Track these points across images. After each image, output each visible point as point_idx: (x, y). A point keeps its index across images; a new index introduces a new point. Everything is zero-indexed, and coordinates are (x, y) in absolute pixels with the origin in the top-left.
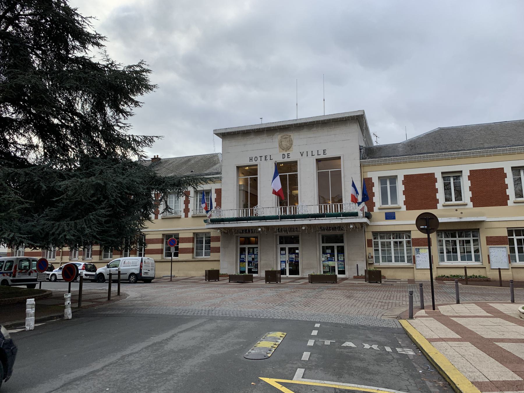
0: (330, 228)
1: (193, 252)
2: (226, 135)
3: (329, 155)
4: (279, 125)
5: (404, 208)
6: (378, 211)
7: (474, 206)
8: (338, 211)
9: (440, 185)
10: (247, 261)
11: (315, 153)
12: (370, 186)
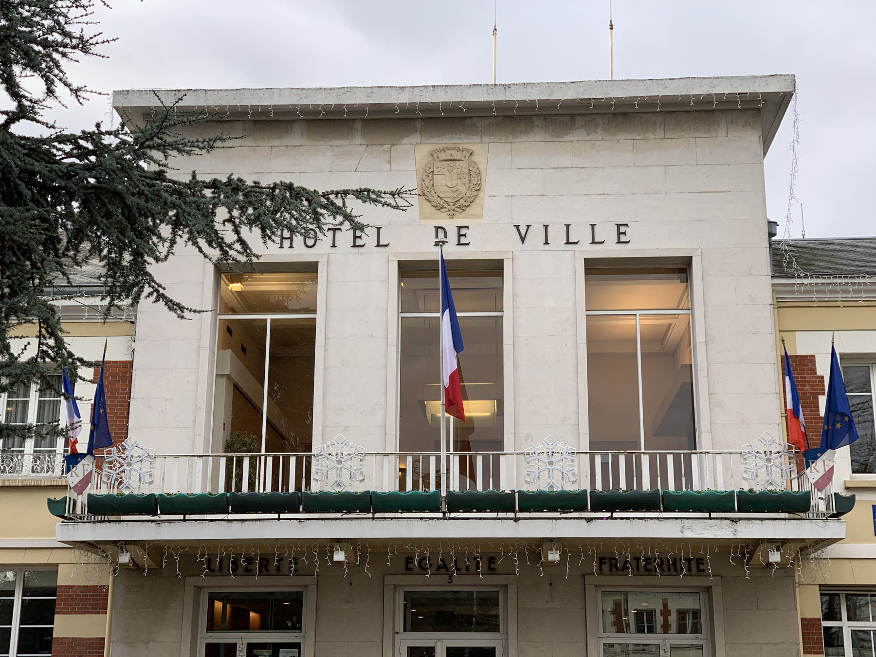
0: (249, 560)
3: (643, 244)
8: (239, 487)
11: (581, 234)
12: (808, 388)
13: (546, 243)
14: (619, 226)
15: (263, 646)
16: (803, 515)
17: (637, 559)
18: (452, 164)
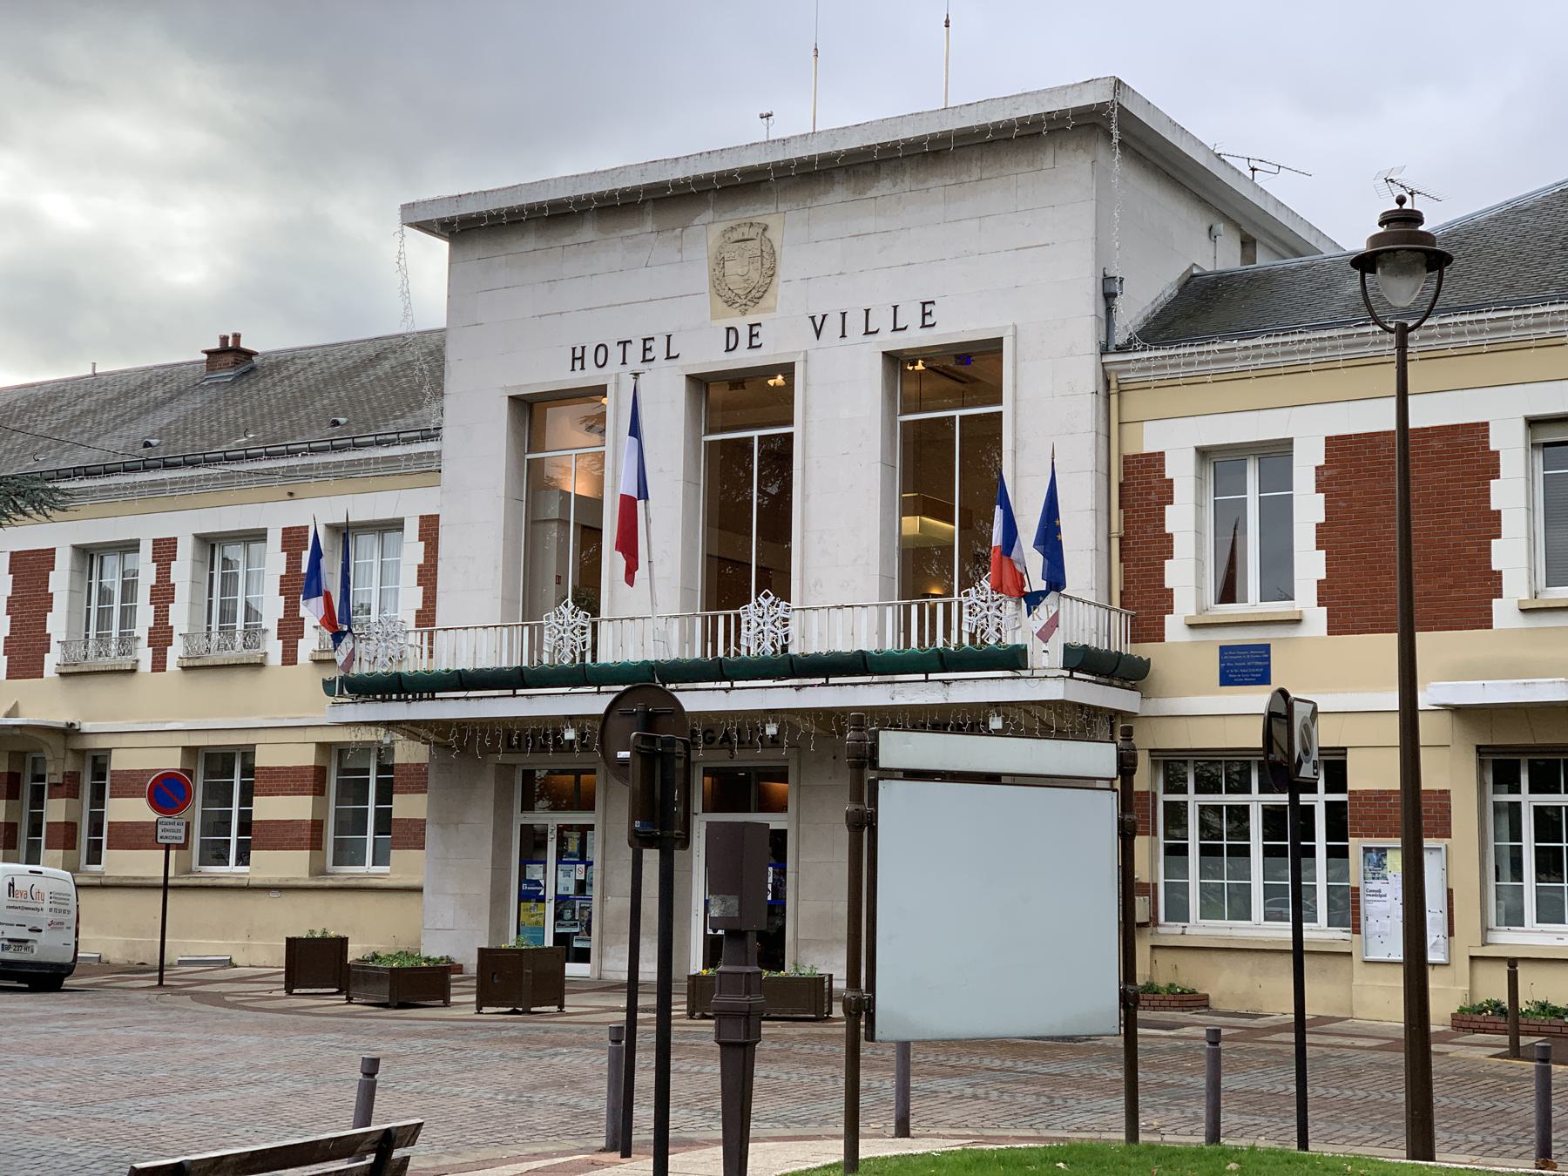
1: (316, 844)
2: (467, 229)
4: (582, 191)
5: (1317, 618)
6: (1521, 622)
7: (1332, 630)
9: (1513, 493)
10: (550, 894)
11: (881, 320)
12: (1153, 497)
13: (843, 336)
14: (924, 304)
15: (570, 827)
18: (742, 244)
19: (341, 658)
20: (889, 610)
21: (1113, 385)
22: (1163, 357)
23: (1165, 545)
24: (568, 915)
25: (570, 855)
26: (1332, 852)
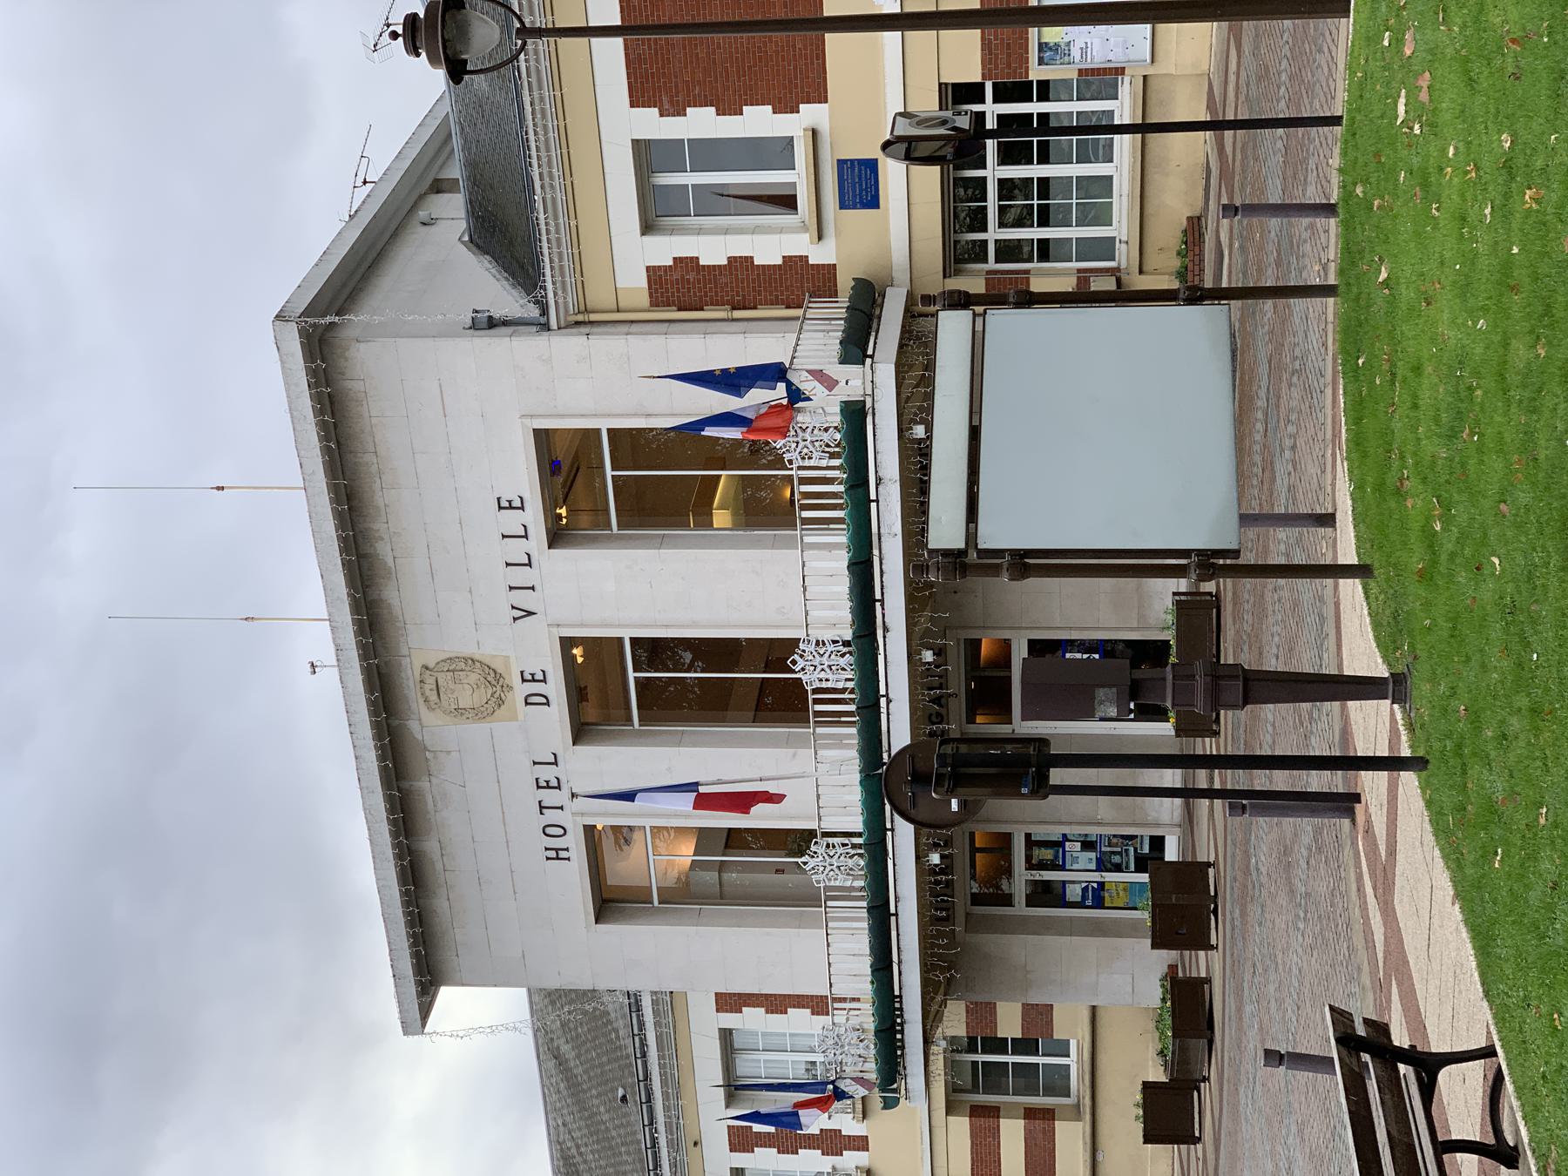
1: (1048, 1115)
2: (427, 969)
3: (524, 478)
5: (810, 113)
6: (830, 243)
10: (1096, 876)
12: (691, 276)
13: (533, 588)
15: (1028, 858)
16: (869, 404)
17: (939, 919)
18: (442, 690)
19: (861, 1092)
20: (807, 539)
21: (580, 318)
22: (552, 268)
23: (742, 265)
24: (1116, 859)
25: (1056, 857)
26: (1044, 96)
